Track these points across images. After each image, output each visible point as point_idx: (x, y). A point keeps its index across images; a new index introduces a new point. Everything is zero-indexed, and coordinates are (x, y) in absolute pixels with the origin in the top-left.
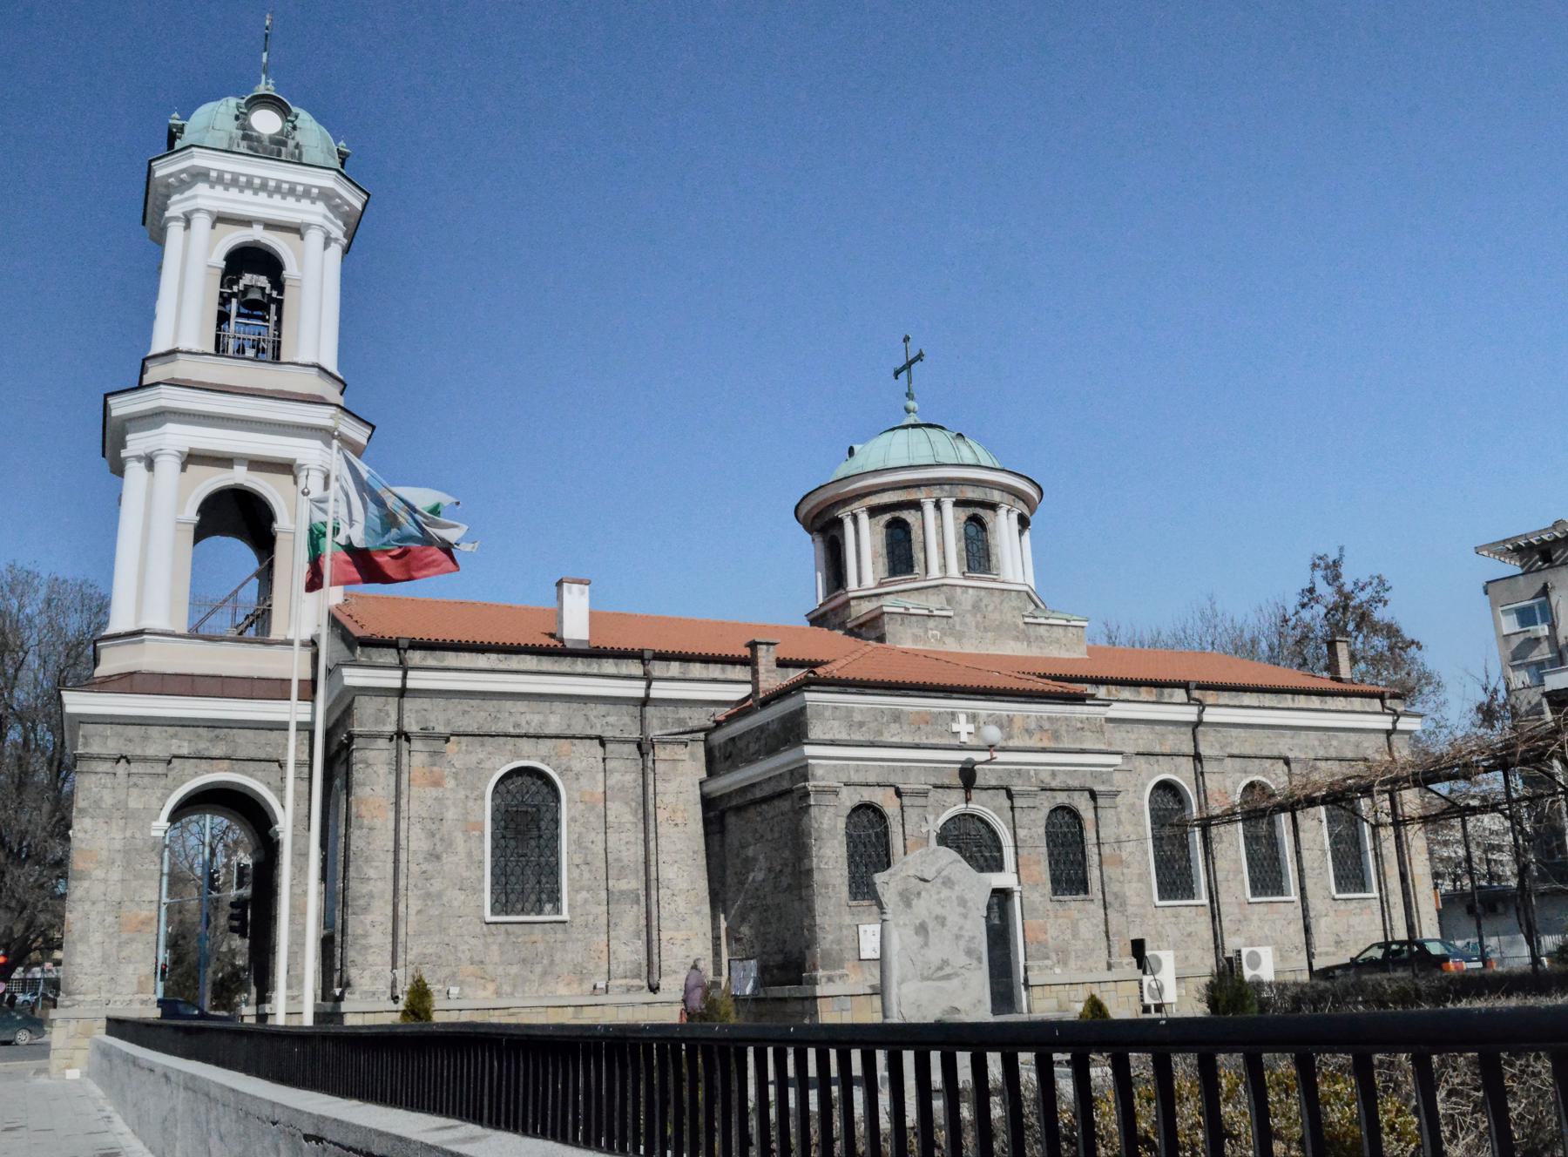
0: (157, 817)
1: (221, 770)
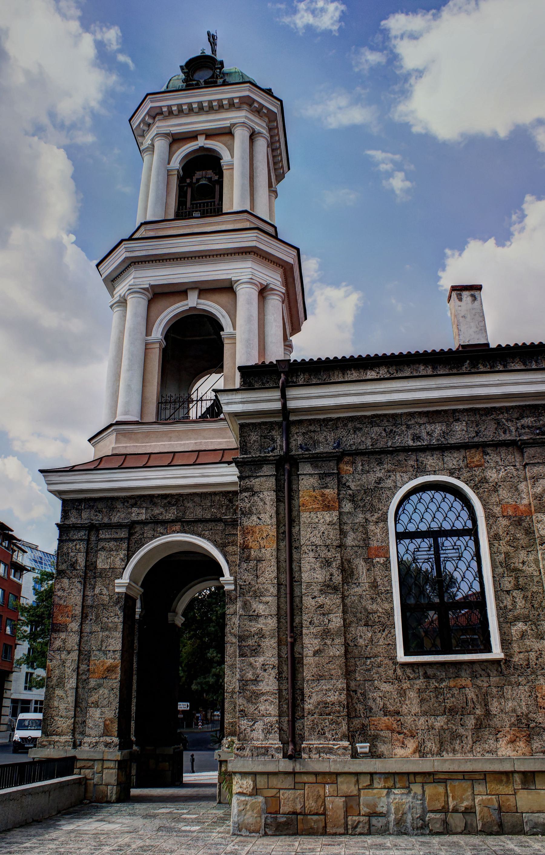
0: (120, 576)
1: (174, 532)
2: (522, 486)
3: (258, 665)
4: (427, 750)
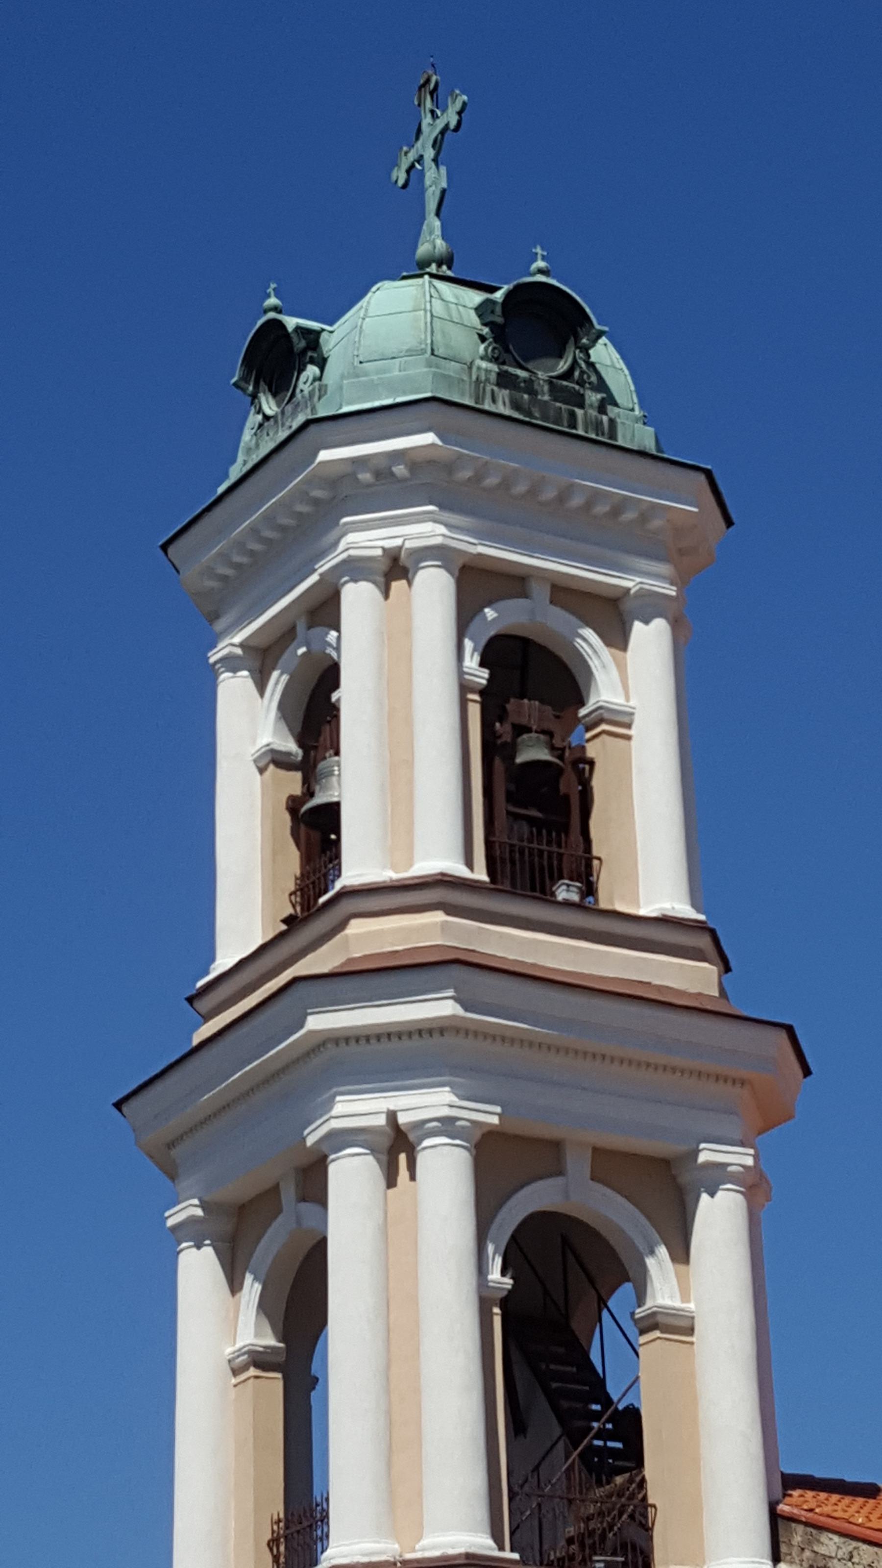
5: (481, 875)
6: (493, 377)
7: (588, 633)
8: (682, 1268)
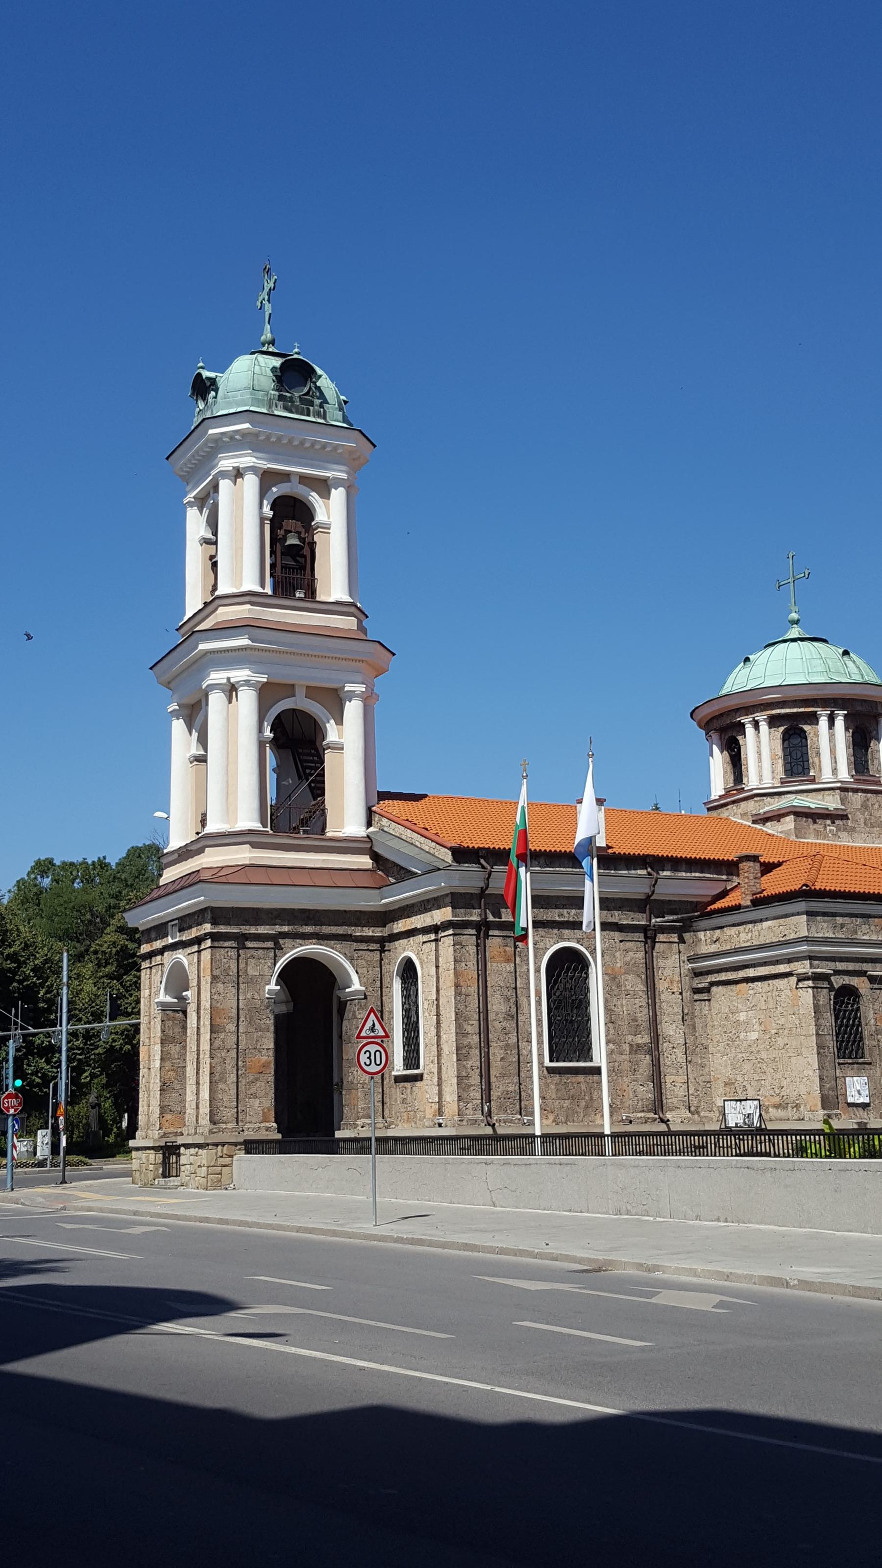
1: (311, 944)
2: (618, 954)
3: (469, 1066)
4: (559, 1120)
5: (268, 590)
6: (277, 397)
7: (314, 494)
8: (340, 727)
